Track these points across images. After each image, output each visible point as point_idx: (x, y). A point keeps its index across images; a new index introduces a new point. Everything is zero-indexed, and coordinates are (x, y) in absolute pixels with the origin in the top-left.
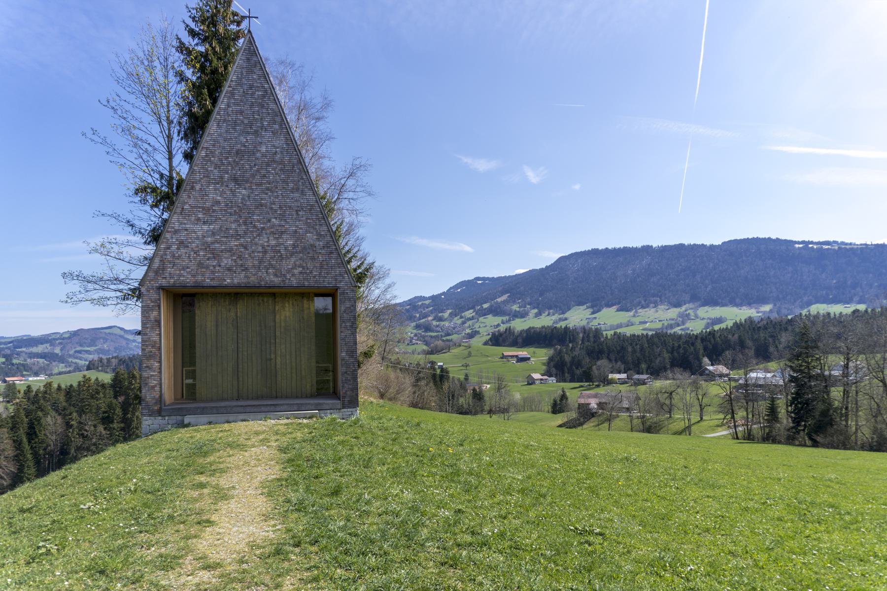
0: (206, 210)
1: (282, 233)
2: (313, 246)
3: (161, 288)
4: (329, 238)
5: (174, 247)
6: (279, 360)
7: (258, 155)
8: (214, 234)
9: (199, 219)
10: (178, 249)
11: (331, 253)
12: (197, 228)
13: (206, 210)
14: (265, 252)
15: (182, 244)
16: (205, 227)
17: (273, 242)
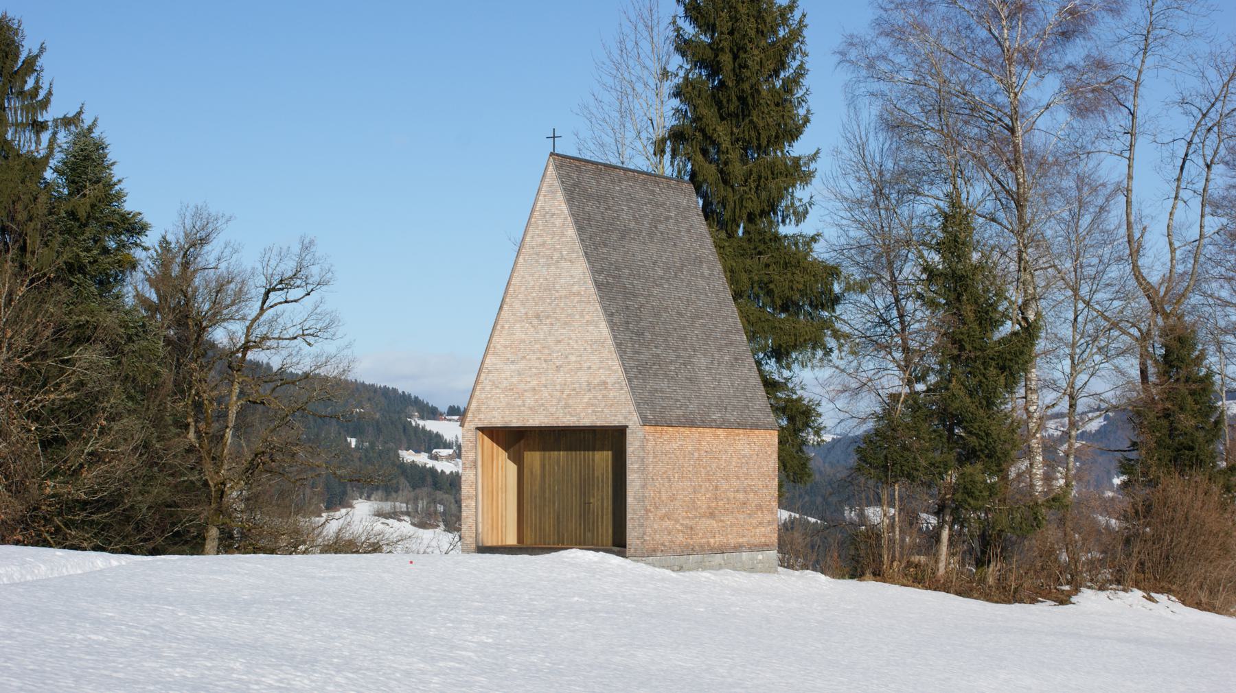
2: (605, 383)
3: (478, 428)
16: (513, 367)
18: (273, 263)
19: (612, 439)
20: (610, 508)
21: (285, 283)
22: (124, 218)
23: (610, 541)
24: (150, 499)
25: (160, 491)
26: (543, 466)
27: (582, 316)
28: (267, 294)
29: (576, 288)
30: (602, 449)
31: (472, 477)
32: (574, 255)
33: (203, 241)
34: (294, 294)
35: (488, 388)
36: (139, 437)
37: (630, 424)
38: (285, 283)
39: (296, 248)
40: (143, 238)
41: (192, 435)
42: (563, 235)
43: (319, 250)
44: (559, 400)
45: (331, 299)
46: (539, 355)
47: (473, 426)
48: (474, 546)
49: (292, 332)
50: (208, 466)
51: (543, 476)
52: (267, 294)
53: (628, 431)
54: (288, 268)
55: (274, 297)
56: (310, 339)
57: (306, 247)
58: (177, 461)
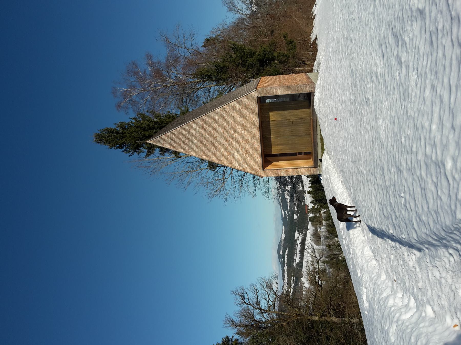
0: (229, 154)
1: (235, 123)
2: (239, 109)
3: (263, 170)
4: (235, 102)
5: (246, 166)
6: (292, 118)
7: (201, 135)
8: (239, 151)
9: (233, 157)
10: (246, 164)
11: (242, 101)
12: (236, 158)
13: (229, 154)
14: (245, 130)
15: (244, 163)
16: (236, 154)
17: (240, 127)
18: (238, 302)
19: (261, 100)
20: (294, 111)
21: (243, 298)
22: (223, 343)
23: (308, 110)
24: (302, 334)
25: (299, 330)
26: (278, 145)
27: (211, 123)
28: (246, 303)
29: (201, 127)
30: (269, 117)
31: (284, 171)
32: (187, 128)
33: (233, 321)
34: (246, 296)
35: (246, 166)
36: (285, 338)
37: (256, 95)
38: (243, 298)
39: (234, 296)
40: (230, 337)
41: (284, 324)
42: (179, 134)
43: (234, 289)
44: (249, 131)
45: (247, 286)
46: (230, 142)
47: (262, 172)
48: (314, 169)
49: (256, 296)
50: (292, 319)
51: (282, 144)
52: (246, 303)
53: (259, 96)
54: (239, 298)
55: (247, 301)
56: (257, 291)
57: (234, 293)
58: (291, 327)
